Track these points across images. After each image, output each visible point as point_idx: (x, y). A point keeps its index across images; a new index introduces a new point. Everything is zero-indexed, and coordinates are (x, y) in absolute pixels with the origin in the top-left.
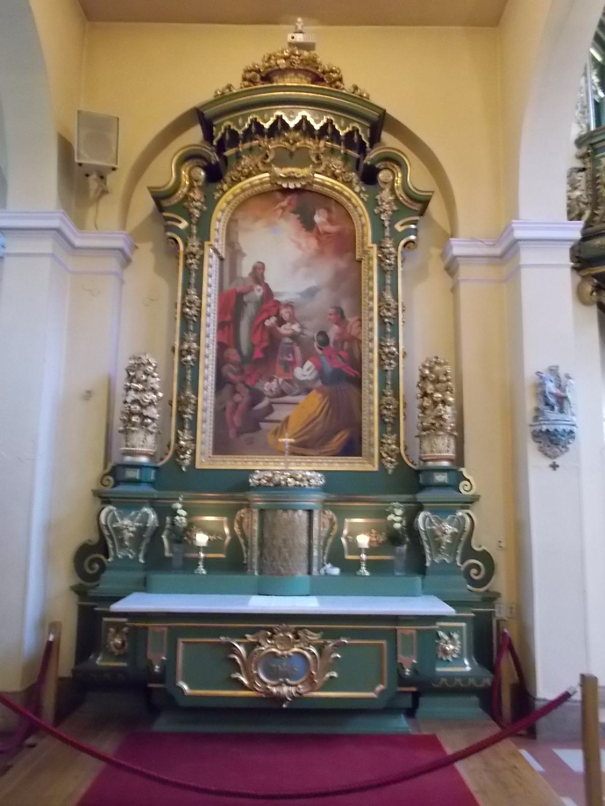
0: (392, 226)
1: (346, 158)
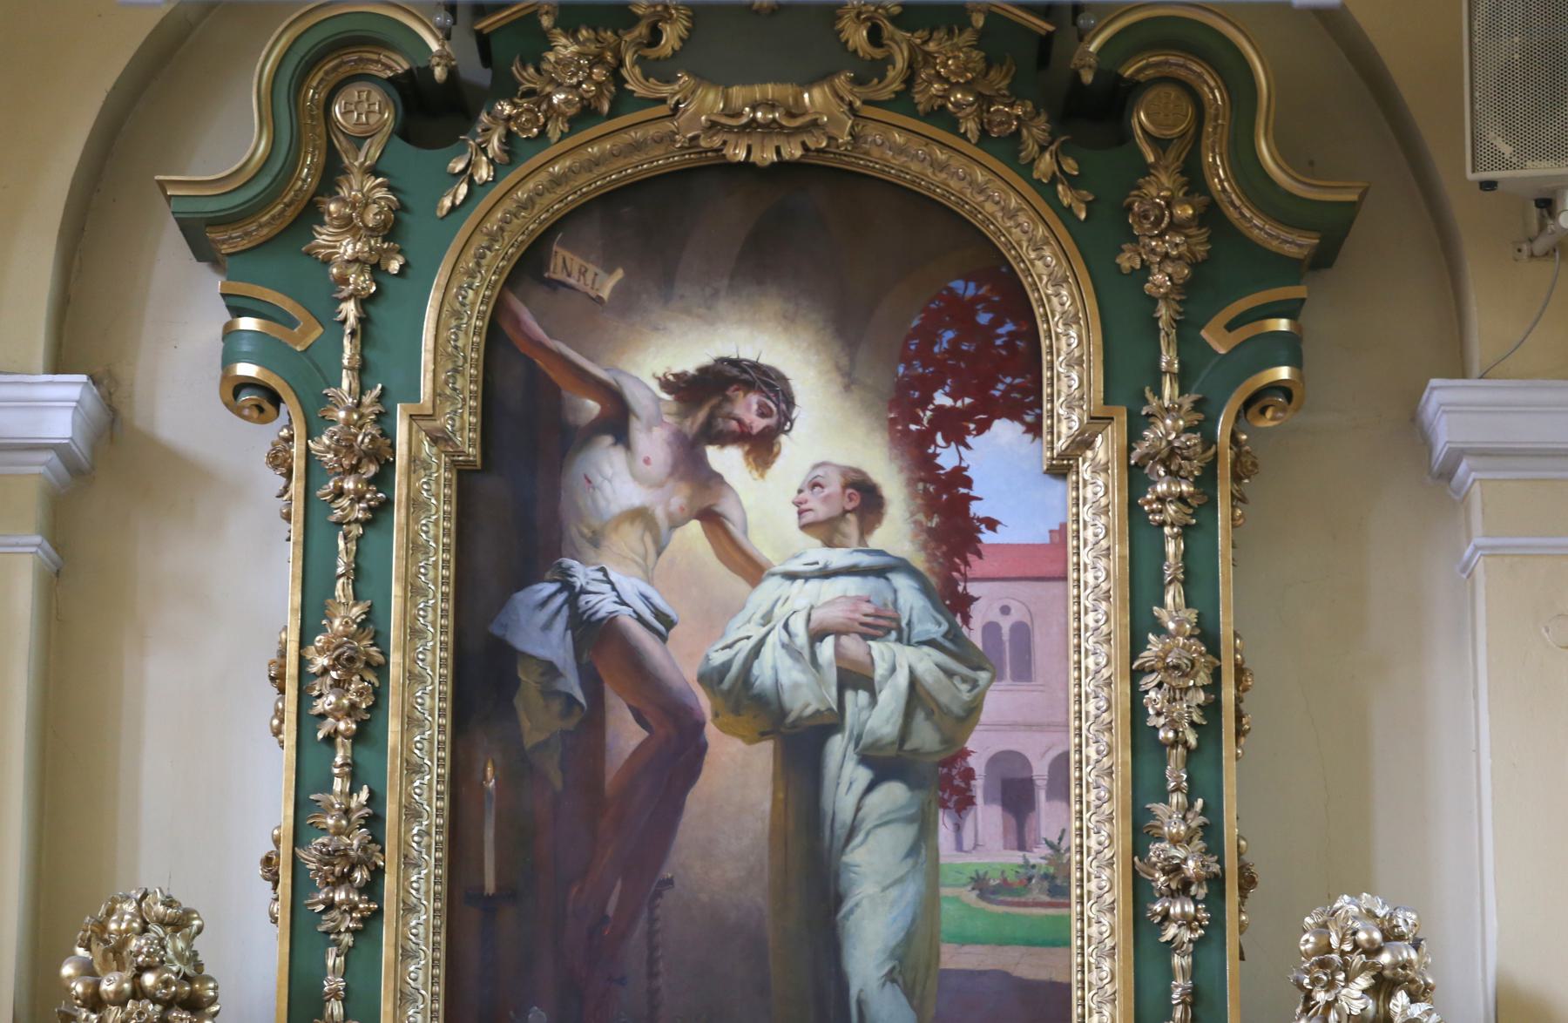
0: (1186, 330)
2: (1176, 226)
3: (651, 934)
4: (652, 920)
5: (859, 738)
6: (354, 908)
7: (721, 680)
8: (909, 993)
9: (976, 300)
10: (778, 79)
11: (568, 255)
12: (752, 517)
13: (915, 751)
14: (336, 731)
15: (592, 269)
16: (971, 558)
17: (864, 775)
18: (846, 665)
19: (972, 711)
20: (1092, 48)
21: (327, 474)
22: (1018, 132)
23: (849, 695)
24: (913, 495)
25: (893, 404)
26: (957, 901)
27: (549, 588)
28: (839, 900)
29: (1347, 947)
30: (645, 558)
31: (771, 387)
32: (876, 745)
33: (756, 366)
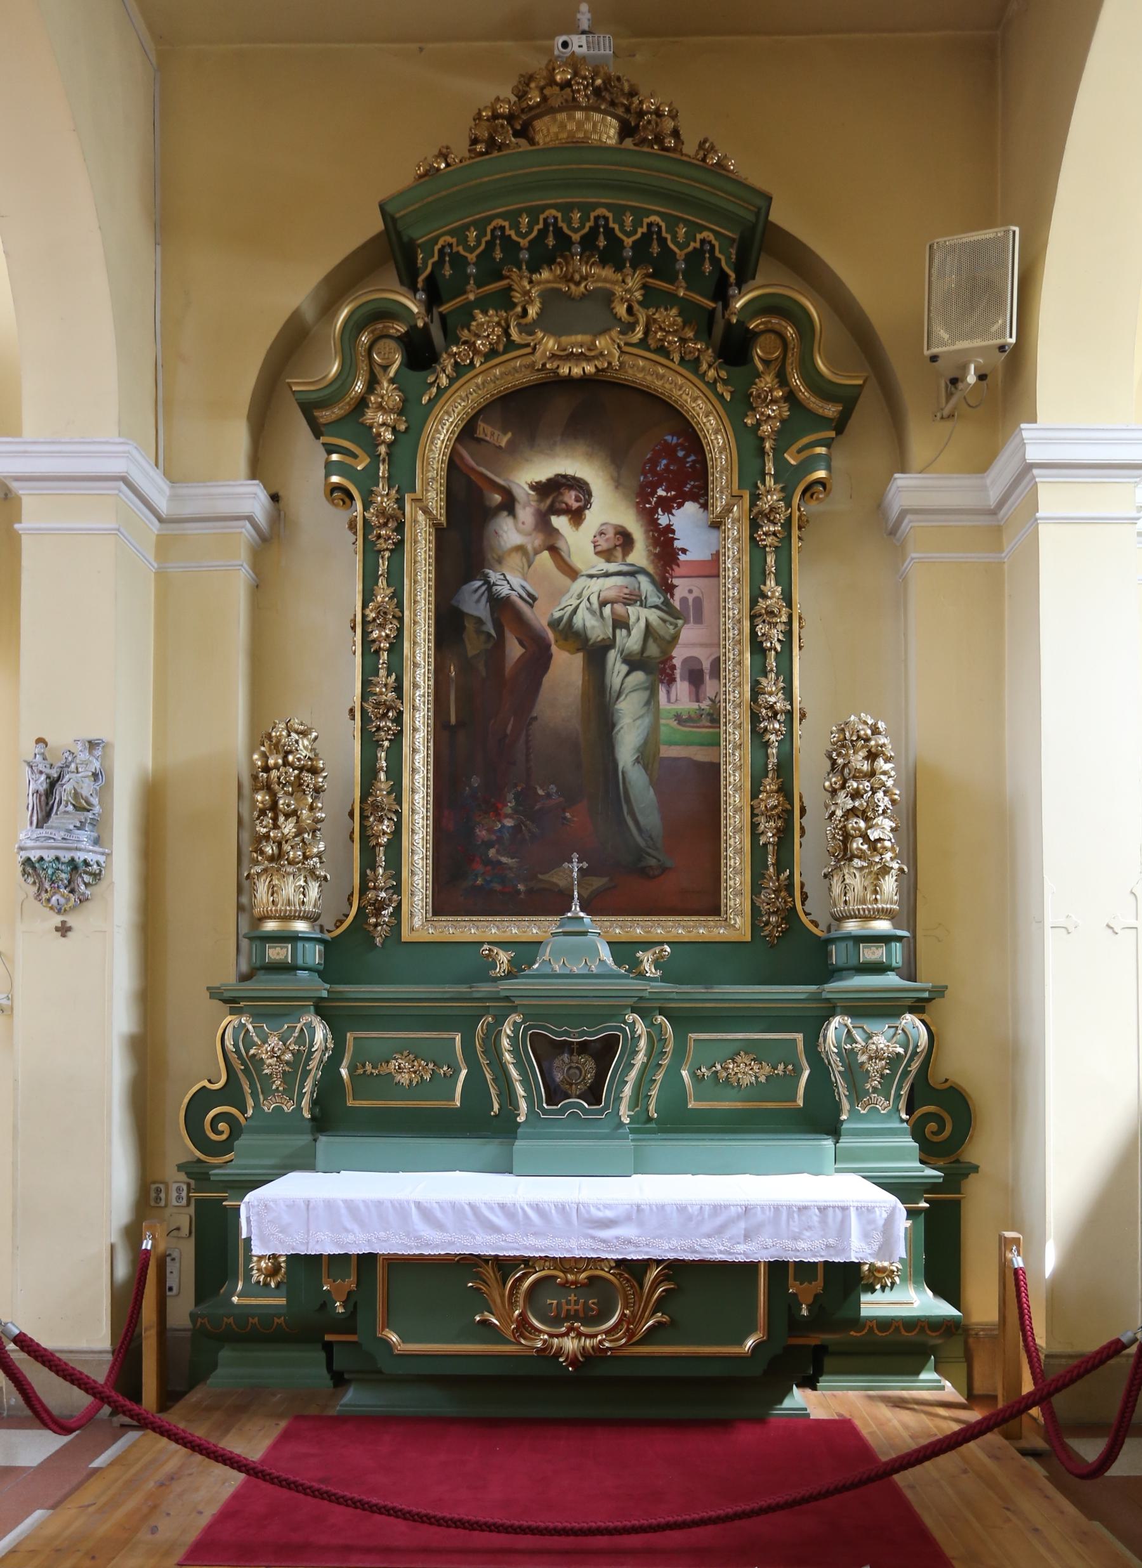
0: (778, 451)
1: (688, 311)
2: (774, 401)
3: (527, 742)
4: (528, 736)
5: (623, 651)
6: (389, 729)
7: (559, 625)
8: (646, 768)
9: (677, 445)
10: (584, 333)
11: (486, 426)
12: (572, 550)
13: (648, 657)
14: (380, 648)
15: (497, 433)
16: (675, 567)
17: (625, 668)
18: (615, 617)
19: (675, 638)
20: (738, 305)
21: (372, 528)
22: (698, 358)
23: (618, 631)
24: (647, 538)
25: (639, 495)
26: (668, 725)
27: (479, 583)
28: (613, 725)
29: (854, 738)
30: (523, 568)
31: (581, 488)
32: (630, 654)
33: (574, 478)
